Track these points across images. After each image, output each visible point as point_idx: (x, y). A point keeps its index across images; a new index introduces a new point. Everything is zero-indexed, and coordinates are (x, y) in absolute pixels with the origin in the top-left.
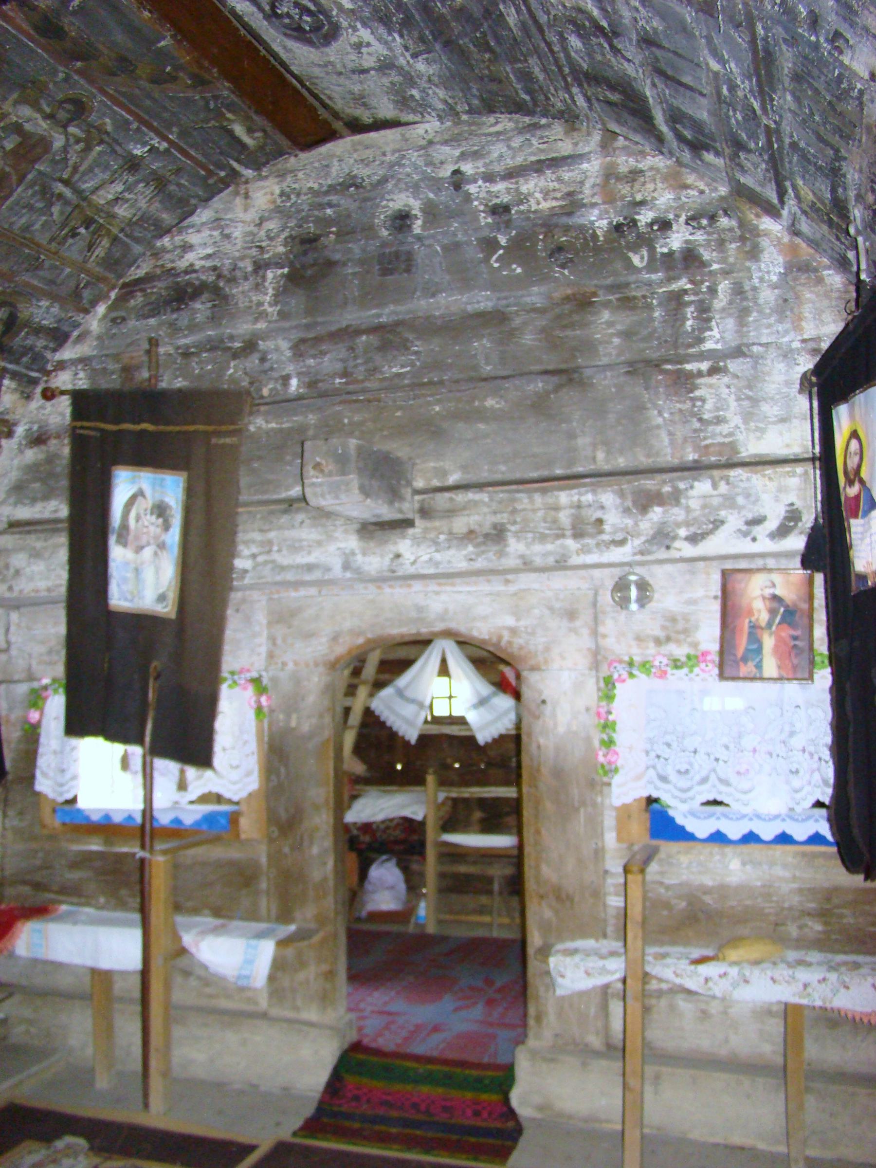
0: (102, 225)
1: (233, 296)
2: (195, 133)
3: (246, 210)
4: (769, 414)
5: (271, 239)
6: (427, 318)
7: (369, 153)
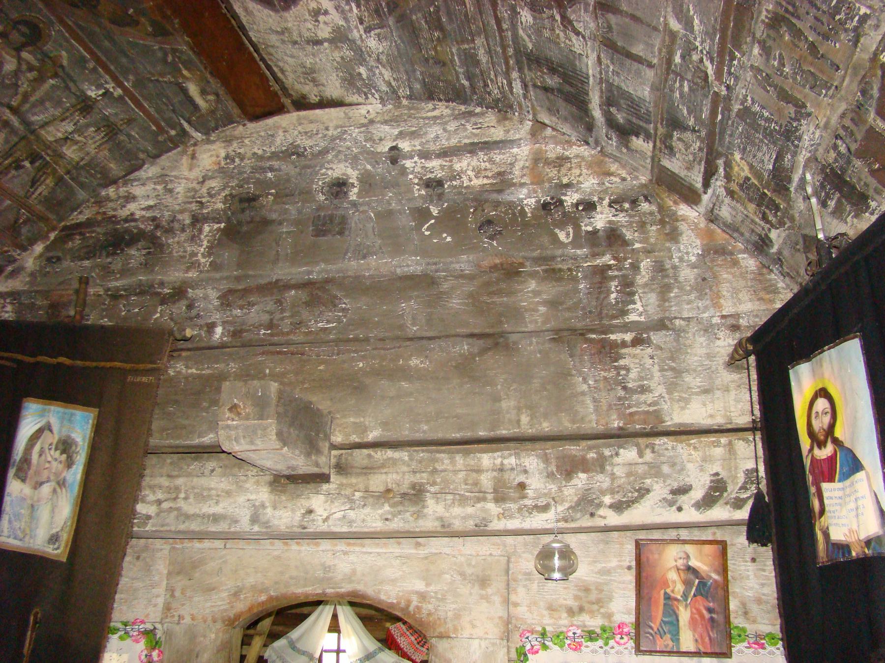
0: (48, 162)
1: (169, 245)
2: (151, 85)
3: (190, 170)
4: (692, 385)
5: (210, 195)
6: (357, 277)
7: (313, 127)
